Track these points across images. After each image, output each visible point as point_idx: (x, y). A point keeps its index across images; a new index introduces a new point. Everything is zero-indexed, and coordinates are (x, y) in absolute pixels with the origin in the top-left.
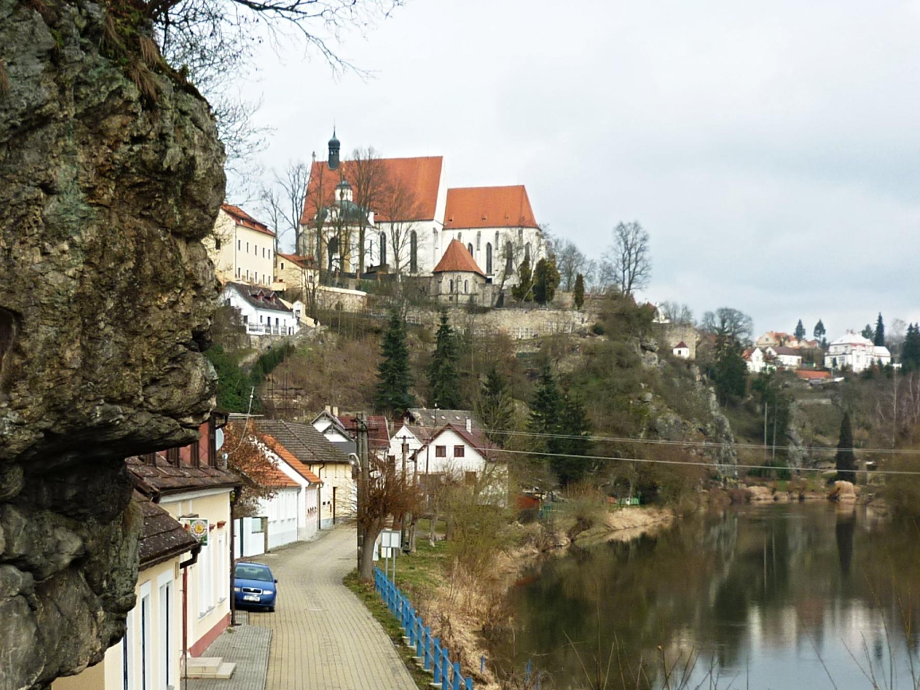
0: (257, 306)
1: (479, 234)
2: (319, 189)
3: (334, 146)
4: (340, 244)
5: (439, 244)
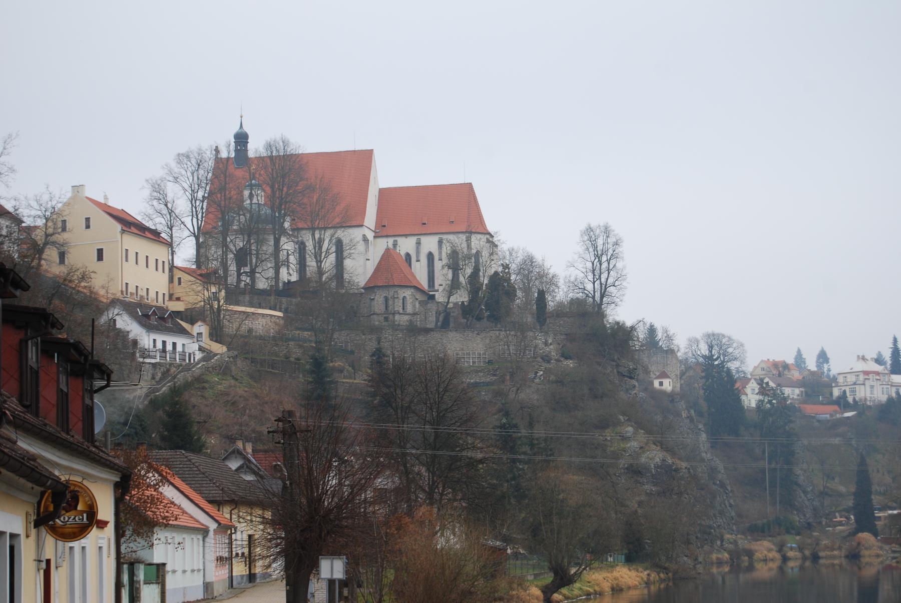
0: (150, 328)
1: (418, 243)
2: (223, 189)
3: (241, 139)
4: (251, 254)
5: (370, 255)
